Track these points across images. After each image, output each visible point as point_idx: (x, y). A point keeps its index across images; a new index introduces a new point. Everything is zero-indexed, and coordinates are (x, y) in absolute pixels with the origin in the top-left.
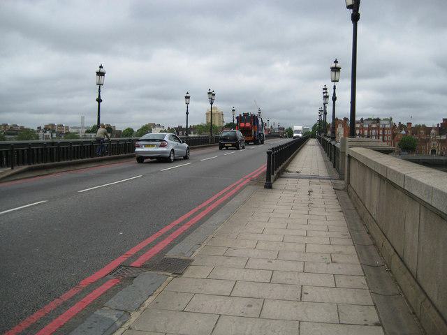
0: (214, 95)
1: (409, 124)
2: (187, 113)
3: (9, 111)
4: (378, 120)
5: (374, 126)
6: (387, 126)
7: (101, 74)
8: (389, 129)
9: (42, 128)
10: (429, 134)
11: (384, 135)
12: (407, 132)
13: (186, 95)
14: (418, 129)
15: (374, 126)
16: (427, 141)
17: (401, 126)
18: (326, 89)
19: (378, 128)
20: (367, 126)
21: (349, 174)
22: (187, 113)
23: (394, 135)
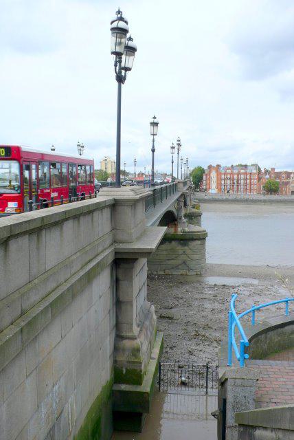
0: (83, 147)
1: (273, 169)
2: (153, 151)
3: (121, 242)
4: (246, 166)
5: (242, 171)
6: (253, 171)
7: (155, 124)
8: (254, 174)
9: (119, 40)
10: (290, 177)
11: (251, 179)
12: (270, 176)
13: (152, 120)
14: (278, 175)
15: (242, 171)
16: (287, 184)
17: (266, 171)
18: (179, 141)
19: (246, 173)
20: (237, 171)
21: (271, 202)
22: (153, 151)
23: (259, 179)
